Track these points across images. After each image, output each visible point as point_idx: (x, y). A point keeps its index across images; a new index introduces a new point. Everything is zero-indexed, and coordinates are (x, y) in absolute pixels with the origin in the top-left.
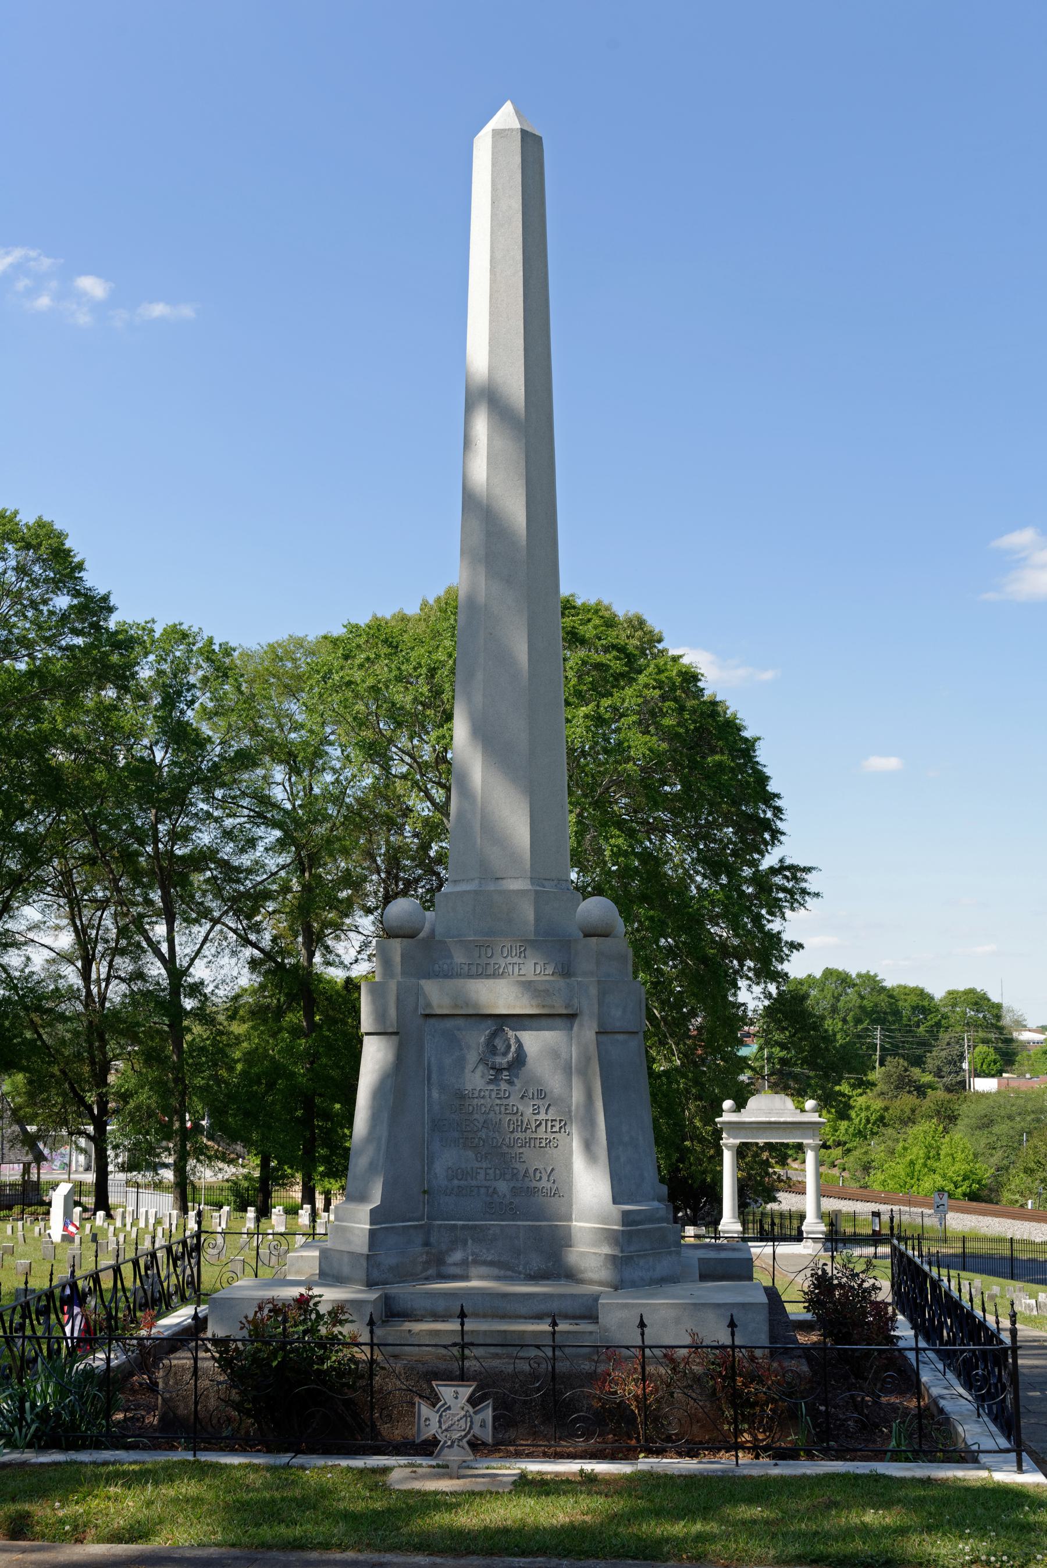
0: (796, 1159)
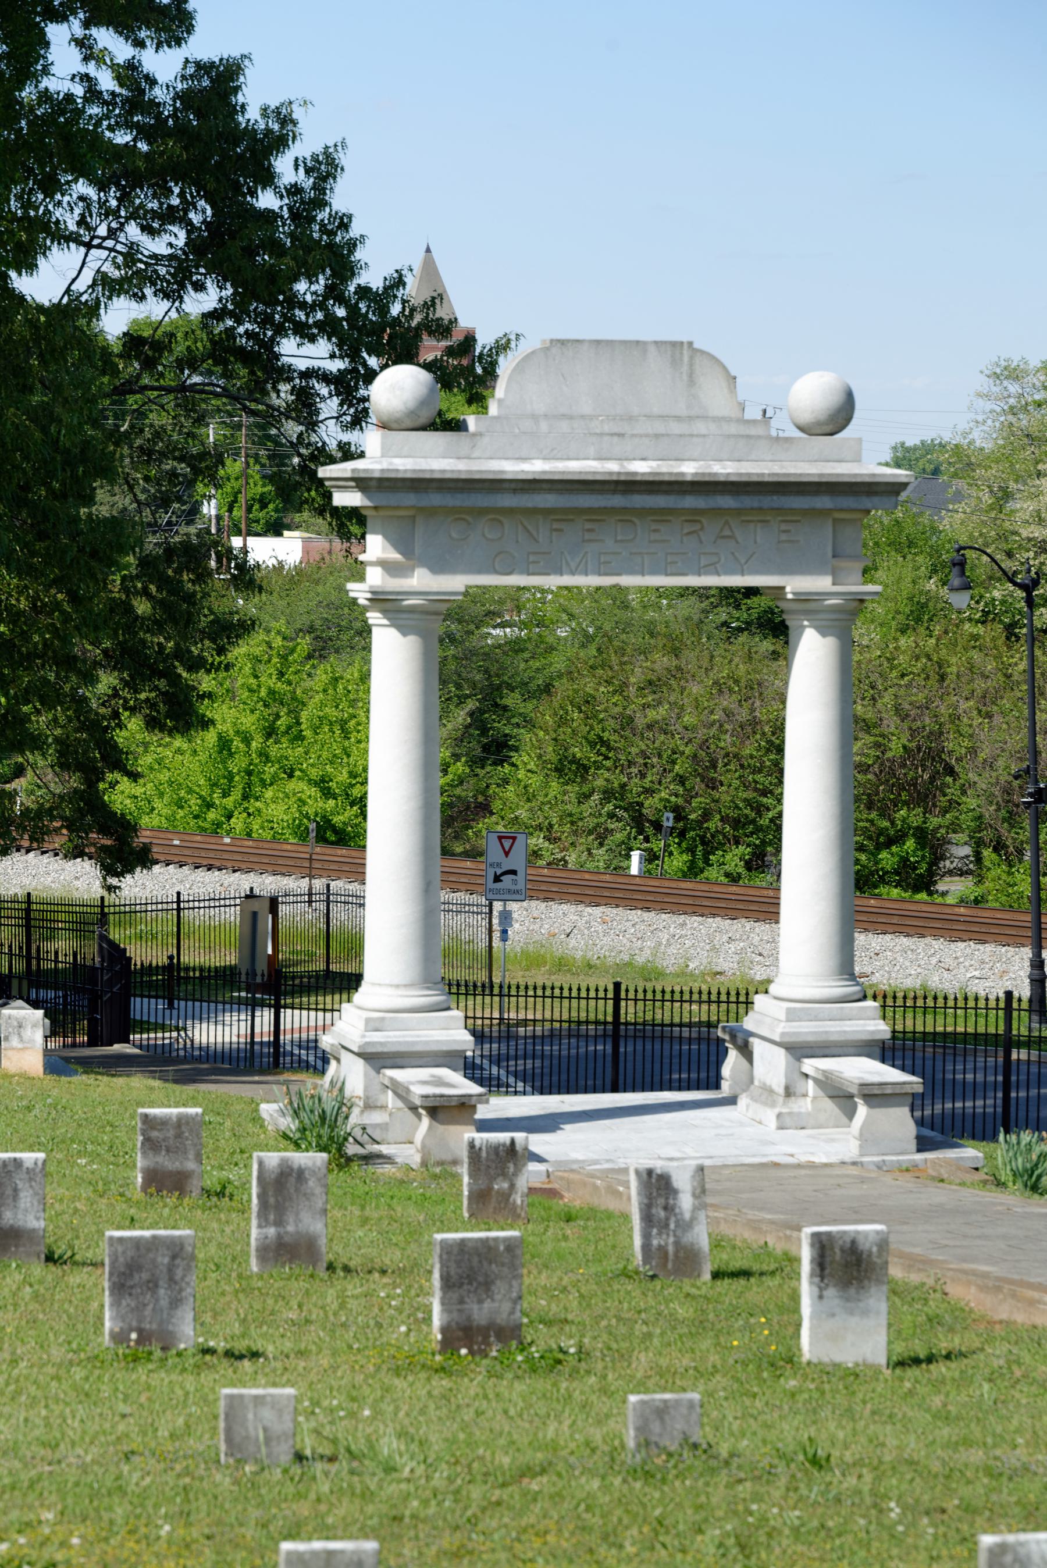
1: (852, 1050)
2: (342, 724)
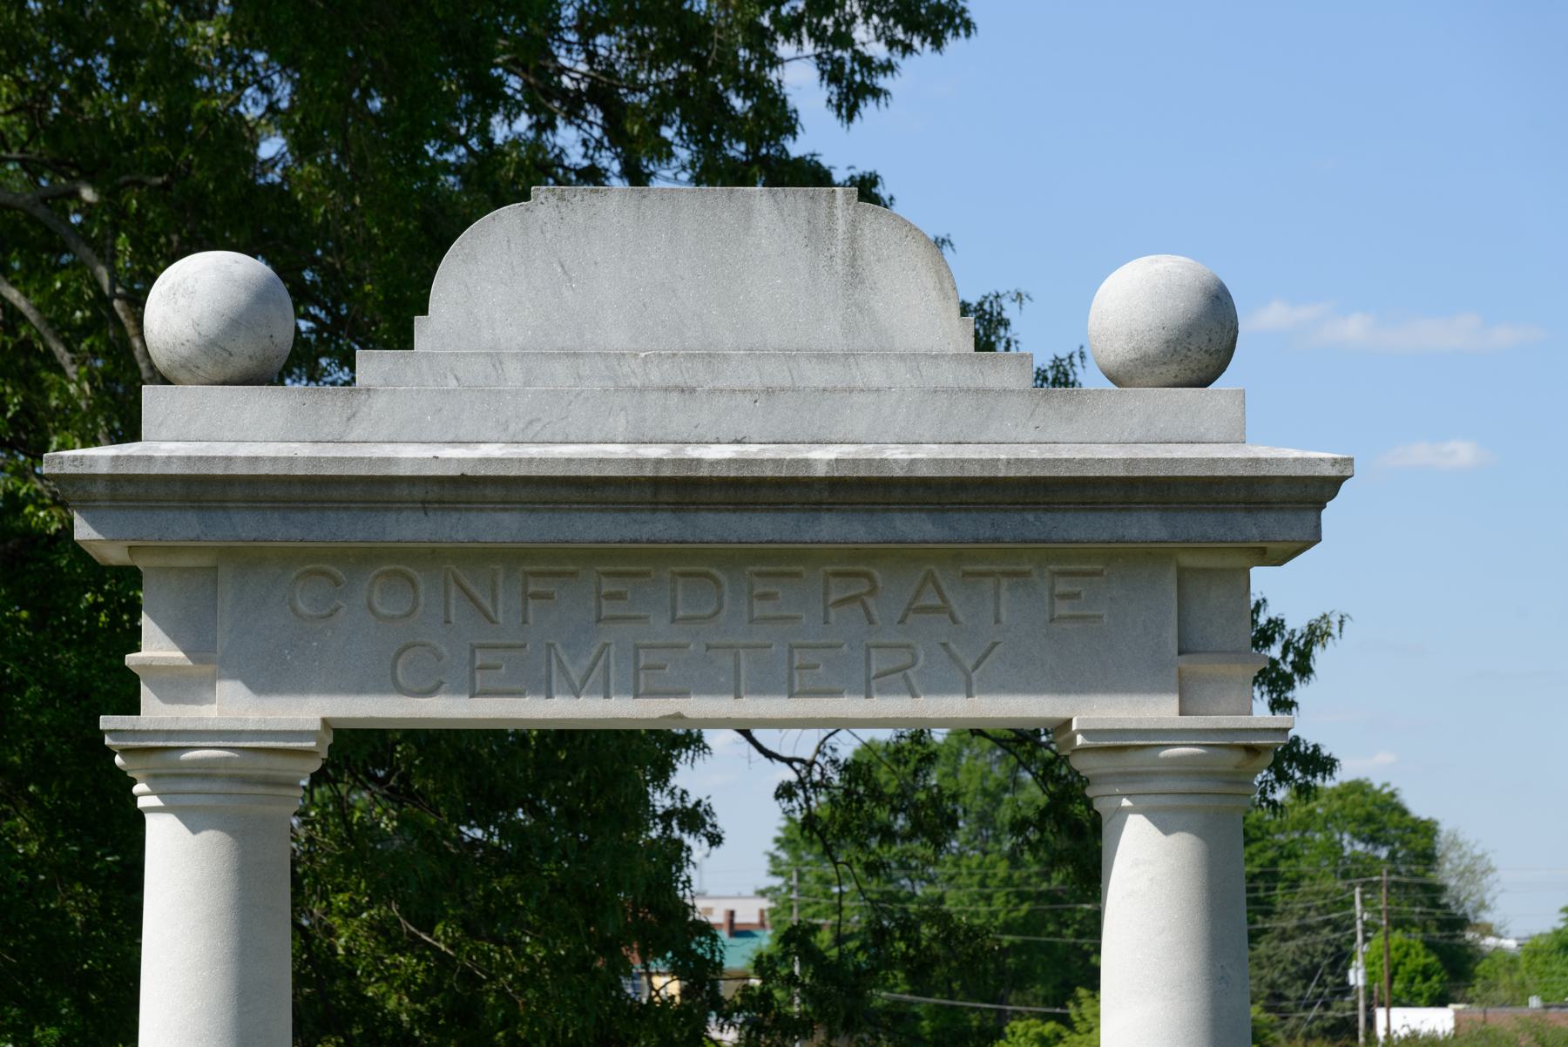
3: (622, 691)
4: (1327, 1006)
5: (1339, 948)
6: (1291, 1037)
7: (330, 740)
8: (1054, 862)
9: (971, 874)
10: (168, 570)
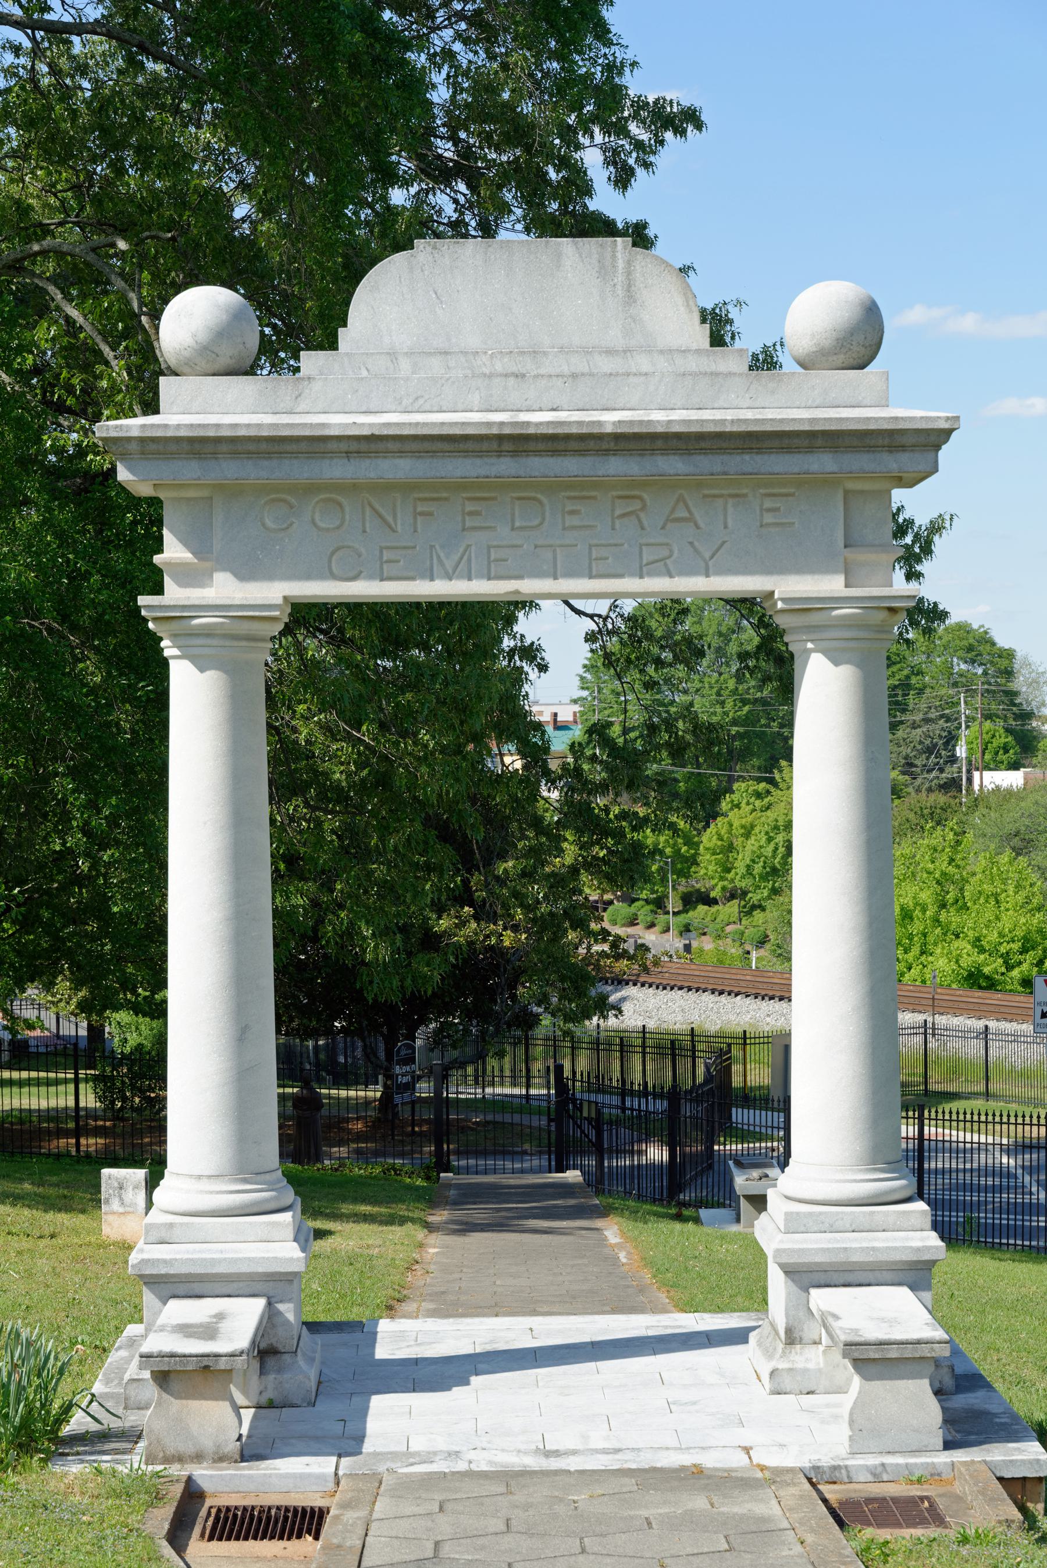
0: (651, 925)
1: (888, 1276)
2: (996, 896)
3: (480, 576)
4: (942, 770)
5: (950, 732)
6: (918, 790)
7: (289, 610)
8: (766, 679)
9: (711, 688)
10: (179, 500)
